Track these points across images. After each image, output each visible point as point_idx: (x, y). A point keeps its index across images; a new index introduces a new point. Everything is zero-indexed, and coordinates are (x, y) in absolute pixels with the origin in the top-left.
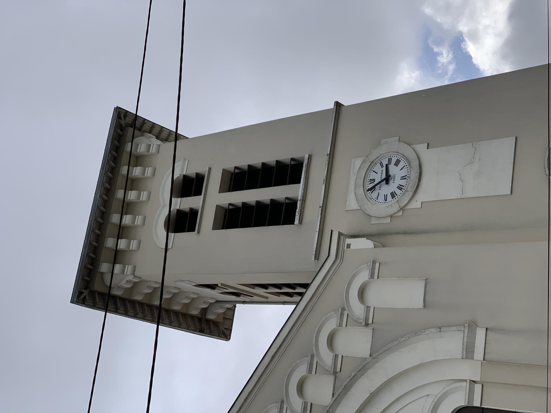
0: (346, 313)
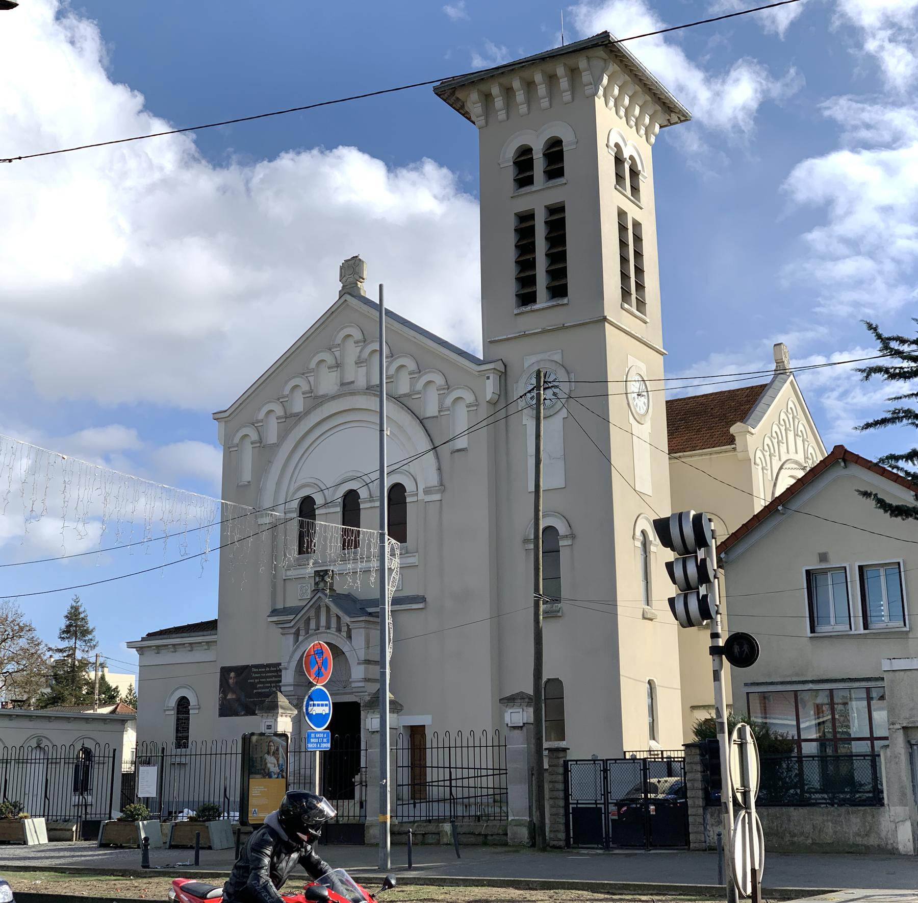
0: (445, 391)
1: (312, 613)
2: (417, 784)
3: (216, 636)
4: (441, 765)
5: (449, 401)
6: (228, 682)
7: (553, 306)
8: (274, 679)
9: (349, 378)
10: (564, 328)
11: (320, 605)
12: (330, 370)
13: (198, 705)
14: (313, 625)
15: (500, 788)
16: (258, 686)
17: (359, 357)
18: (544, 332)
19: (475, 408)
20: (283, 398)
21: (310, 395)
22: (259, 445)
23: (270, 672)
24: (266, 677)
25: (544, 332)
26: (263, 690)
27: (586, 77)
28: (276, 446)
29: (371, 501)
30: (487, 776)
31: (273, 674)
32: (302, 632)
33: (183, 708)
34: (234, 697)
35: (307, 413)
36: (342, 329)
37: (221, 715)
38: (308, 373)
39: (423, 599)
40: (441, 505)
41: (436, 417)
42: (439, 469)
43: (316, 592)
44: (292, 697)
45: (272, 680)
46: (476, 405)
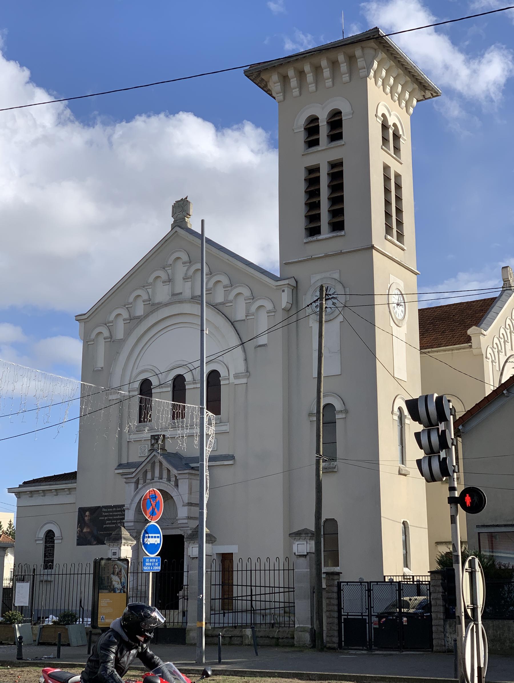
0: (251, 301)
1: (149, 467)
2: (251, 598)
3: (75, 484)
4: (244, 584)
5: (253, 308)
6: (84, 519)
7: (333, 237)
8: (118, 517)
9: (177, 291)
10: (341, 253)
11: (154, 461)
12: (164, 284)
13: (61, 536)
14: (149, 476)
15: (289, 603)
16: (107, 522)
17: (186, 274)
18: (327, 256)
19: (273, 314)
20: (128, 305)
21: (148, 303)
22: (109, 340)
23: (116, 511)
24: (113, 516)
25: (327, 256)
26: (111, 526)
27: (361, 63)
28: (122, 341)
29: (194, 383)
30: (279, 593)
31: (119, 513)
32: (141, 482)
33: (50, 538)
34: (88, 530)
35: (146, 316)
36: (173, 253)
37: (78, 544)
38: (147, 286)
39: (232, 457)
40: (247, 386)
41: (244, 320)
42: (246, 360)
43: (152, 451)
44: (133, 531)
45: (117, 517)
46: (275, 312)
